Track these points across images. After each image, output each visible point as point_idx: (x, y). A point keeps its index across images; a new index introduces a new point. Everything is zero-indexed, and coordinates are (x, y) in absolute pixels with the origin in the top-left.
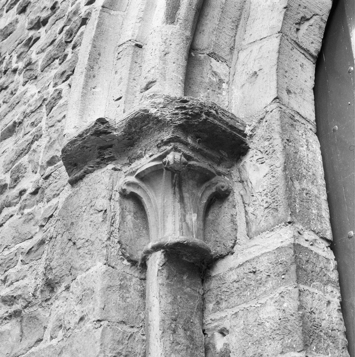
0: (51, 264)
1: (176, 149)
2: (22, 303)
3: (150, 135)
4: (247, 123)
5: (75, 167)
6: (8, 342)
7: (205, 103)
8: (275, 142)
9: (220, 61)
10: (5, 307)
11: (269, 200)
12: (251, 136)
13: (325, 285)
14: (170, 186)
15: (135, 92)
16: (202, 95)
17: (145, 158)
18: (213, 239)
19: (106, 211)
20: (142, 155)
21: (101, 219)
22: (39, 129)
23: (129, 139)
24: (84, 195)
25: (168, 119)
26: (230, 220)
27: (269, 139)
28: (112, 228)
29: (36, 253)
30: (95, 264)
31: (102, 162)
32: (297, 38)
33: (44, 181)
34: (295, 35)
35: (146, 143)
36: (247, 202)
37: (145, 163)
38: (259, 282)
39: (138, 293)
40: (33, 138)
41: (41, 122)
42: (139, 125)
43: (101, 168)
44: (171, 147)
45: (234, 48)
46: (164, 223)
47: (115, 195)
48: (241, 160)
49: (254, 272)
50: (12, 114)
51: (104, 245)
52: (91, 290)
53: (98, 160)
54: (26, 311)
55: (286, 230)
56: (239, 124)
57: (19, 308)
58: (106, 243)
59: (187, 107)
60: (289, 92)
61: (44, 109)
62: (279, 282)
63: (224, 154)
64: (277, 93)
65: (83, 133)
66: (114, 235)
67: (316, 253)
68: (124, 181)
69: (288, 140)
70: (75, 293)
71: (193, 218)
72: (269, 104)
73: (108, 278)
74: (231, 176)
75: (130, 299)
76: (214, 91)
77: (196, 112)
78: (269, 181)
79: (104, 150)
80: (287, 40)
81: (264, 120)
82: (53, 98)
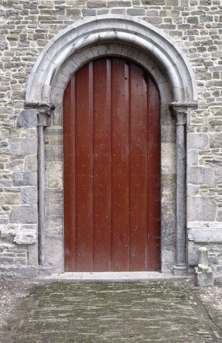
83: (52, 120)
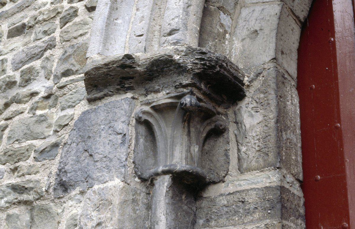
0: (66, 167)
1: (192, 93)
2: (35, 196)
3: (170, 75)
4: (246, 74)
5: (95, 88)
6: (16, 225)
7: (219, 57)
8: (270, 97)
9: (226, 14)
10: (14, 194)
11: (260, 145)
12: (248, 86)
13: (297, 219)
14: (181, 120)
15: (154, 31)
16: (210, 43)
17: (161, 93)
18: (207, 166)
19: (125, 135)
20: (159, 91)
21: (120, 141)
22: (53, 39)
23: (149, 75)
24: (102, 115)
25: (190, 67)
26: (224, 154)
27: (265, 93)
28: (129, 150)
29: (49, 153)
30: (112, 179)
31: (123, 88)
32: (293, 7)
33: (58, 90)
34: (292, 4)
35: (164, 82)
36: (240, 142)
37: (162, 97)
38: (247, 211)
39: (145, 206)
40: (47, 46)
41: (54, 32)
42: (161, 66)
43: (120, 94)
44: (188, 91)
45: (237, 4)
46: (173, 151)
47: (132, 120)
48: (237, 104)
49: (243, 202)
50: (21, 15)
51: (122, 165)
52: (109, 201)
53: (119, 87)
54: (38, 203)
55: (275, 173)
56: (240, 75)
57: (31, 199)
58: (124, 163)
59: (205, 59)
60: (282, 53)
61: (57, 21)
62: (266, 215)
63: (225, 97)
64: (275, 55)
65: (110, 63)
66: (130, 156)
67: (293, 193)
68: (141, 109)
69: (280, 96)
70: (92, 200)
71: (196, 149)
72: (267, 62)
73: (125, 193)
74: (227, 117)
75: (139, 211)
76: (220, 41)
77: (213, 64)
78: (262, 129)
79: (126, 80)
80: (286, 8)
81: (262, 75)
82: (69, 14)
83: (233, 147)
